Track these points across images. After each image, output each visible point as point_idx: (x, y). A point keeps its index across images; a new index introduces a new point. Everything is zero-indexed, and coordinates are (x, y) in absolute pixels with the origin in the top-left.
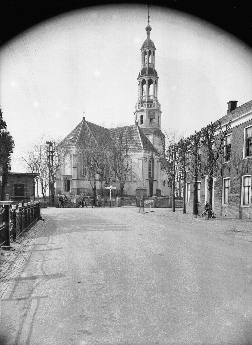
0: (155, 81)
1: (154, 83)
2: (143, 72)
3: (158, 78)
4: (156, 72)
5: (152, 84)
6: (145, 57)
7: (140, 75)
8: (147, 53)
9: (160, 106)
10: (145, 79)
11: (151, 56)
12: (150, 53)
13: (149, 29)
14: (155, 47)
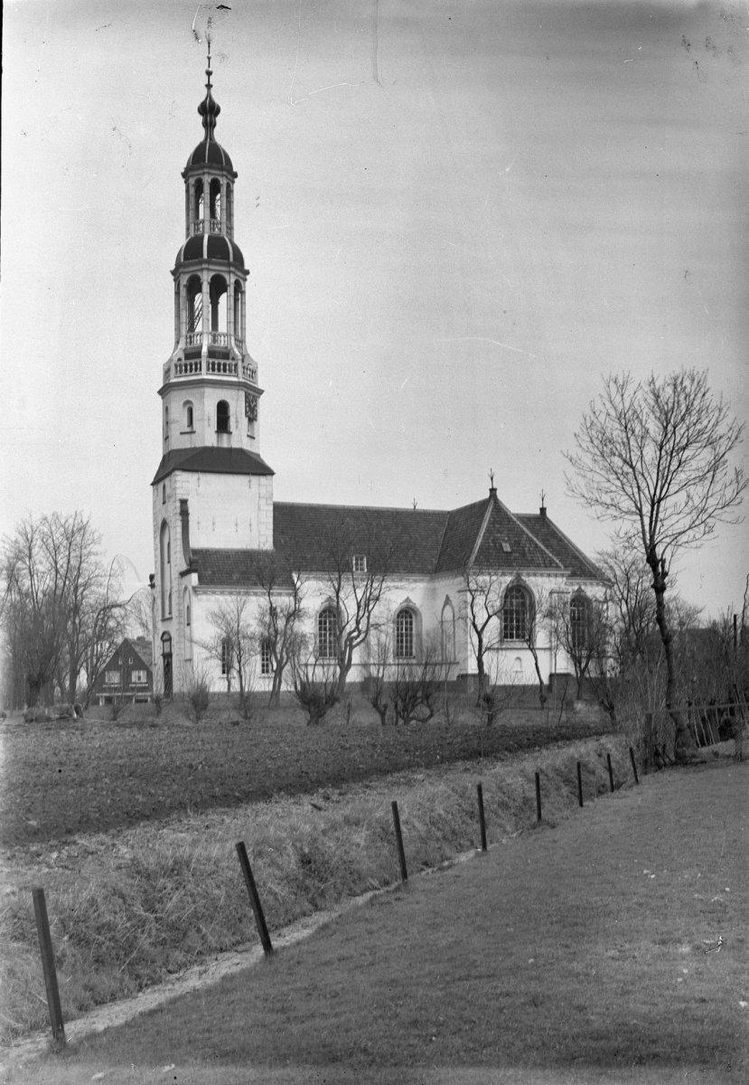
0: (228, 186)
1: (231, 289)
2: (192, 251)
3: (235, 175)
4: (238, 248)
5: (226, 291)
6: (191, 300)
7: (182, 260)
8: (207, 189)
9: (254, 372)
10: (199, 274)
11: (223, 299)
12: (215, 188)
13: (209, 111)
14: (246, 267)
